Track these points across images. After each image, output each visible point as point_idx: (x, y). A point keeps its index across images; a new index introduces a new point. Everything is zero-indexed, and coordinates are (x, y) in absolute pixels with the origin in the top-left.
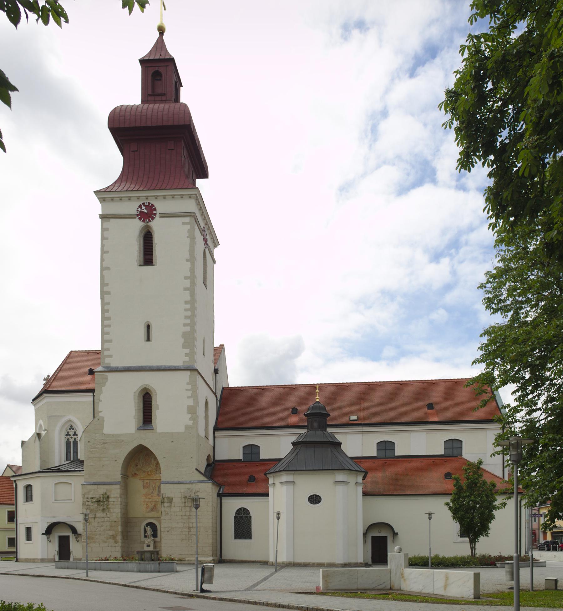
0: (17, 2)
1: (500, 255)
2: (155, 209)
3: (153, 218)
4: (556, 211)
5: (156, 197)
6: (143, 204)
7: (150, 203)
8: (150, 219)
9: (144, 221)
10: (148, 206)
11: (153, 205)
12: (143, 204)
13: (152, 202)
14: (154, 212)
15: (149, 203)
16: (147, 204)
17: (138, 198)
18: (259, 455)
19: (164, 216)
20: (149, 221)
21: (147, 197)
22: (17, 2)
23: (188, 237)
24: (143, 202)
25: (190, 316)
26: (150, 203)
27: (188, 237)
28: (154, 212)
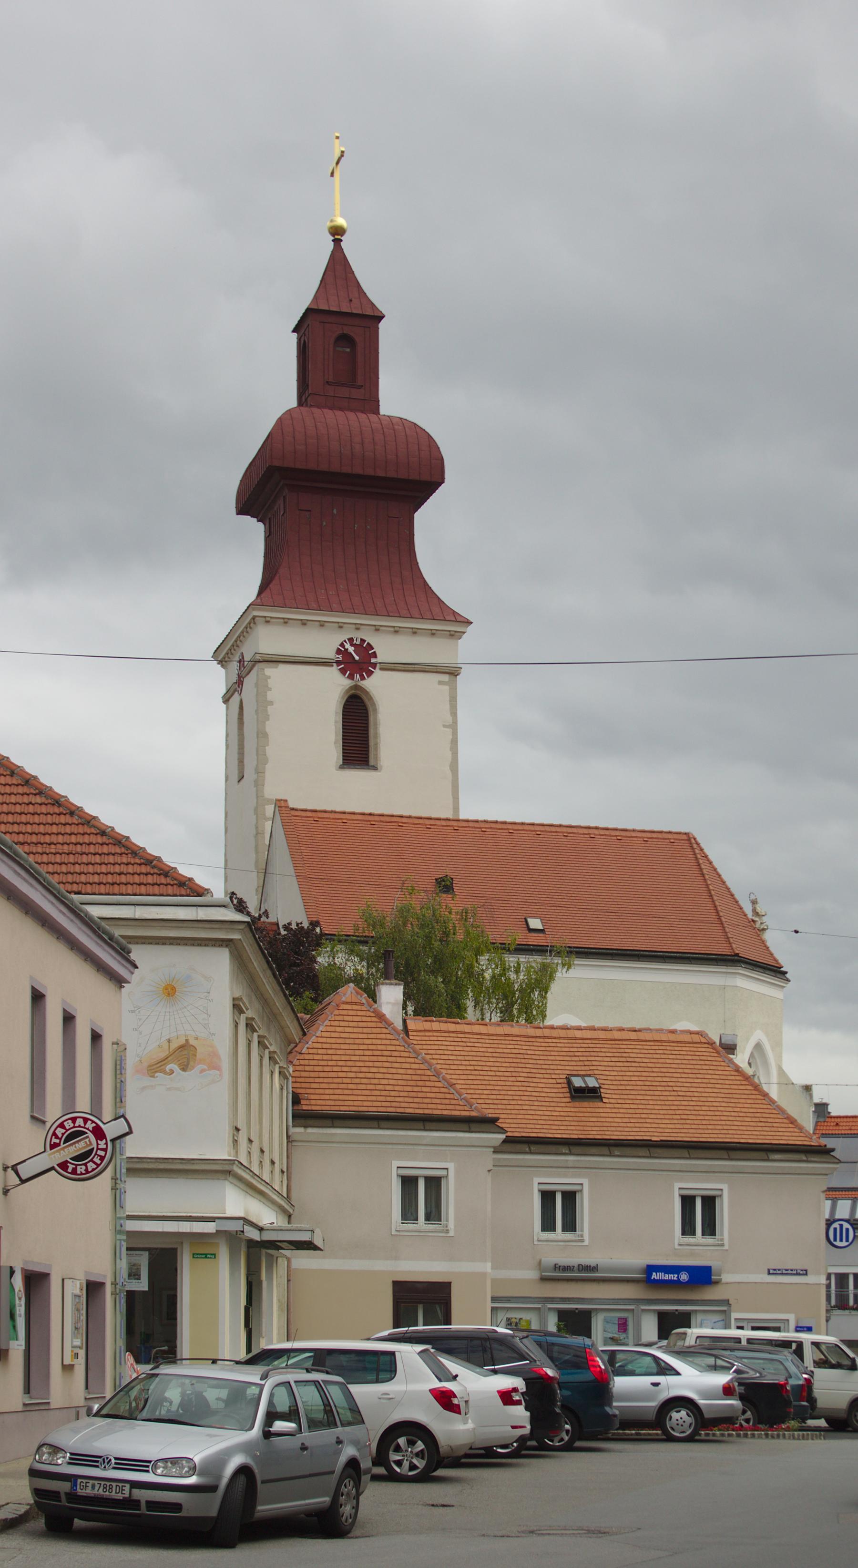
0: (546, 1440)
1: (376, 1478)
2: (375, 655)
3: (370, 673)
4: (326, 1026)
5: (377, 629)
6: (351, 640)
7: (365, 641)
8: (364, 673)
9: (351, 677)
10: (361, 645)
11: (370, 647)
12: (349, 639)
13: (369, 639)
14: (373, 660)
15: (363, 641)
16: (358, 643)
17: (341, 626)
18: (457, 756)
19: (391, 667)
20: (363, 678)
21: (358, 627)
22: (546, 1440)
23: (271, 703)
24: (350, 636)
25: (453, 729)
26: (365, 641)
27: (271, 703)
28: (373, 660)
